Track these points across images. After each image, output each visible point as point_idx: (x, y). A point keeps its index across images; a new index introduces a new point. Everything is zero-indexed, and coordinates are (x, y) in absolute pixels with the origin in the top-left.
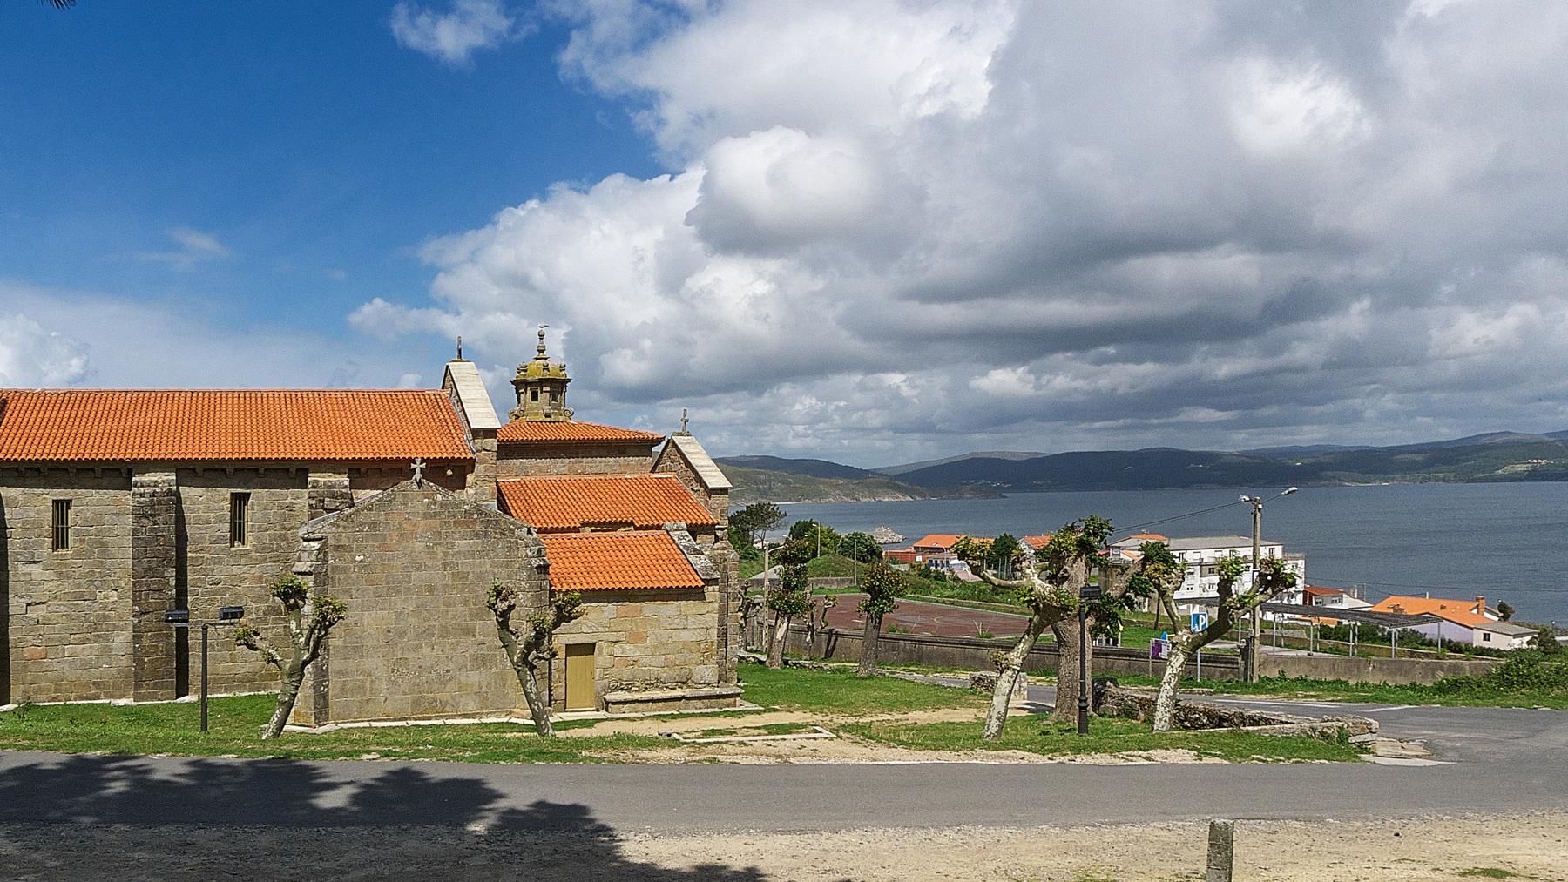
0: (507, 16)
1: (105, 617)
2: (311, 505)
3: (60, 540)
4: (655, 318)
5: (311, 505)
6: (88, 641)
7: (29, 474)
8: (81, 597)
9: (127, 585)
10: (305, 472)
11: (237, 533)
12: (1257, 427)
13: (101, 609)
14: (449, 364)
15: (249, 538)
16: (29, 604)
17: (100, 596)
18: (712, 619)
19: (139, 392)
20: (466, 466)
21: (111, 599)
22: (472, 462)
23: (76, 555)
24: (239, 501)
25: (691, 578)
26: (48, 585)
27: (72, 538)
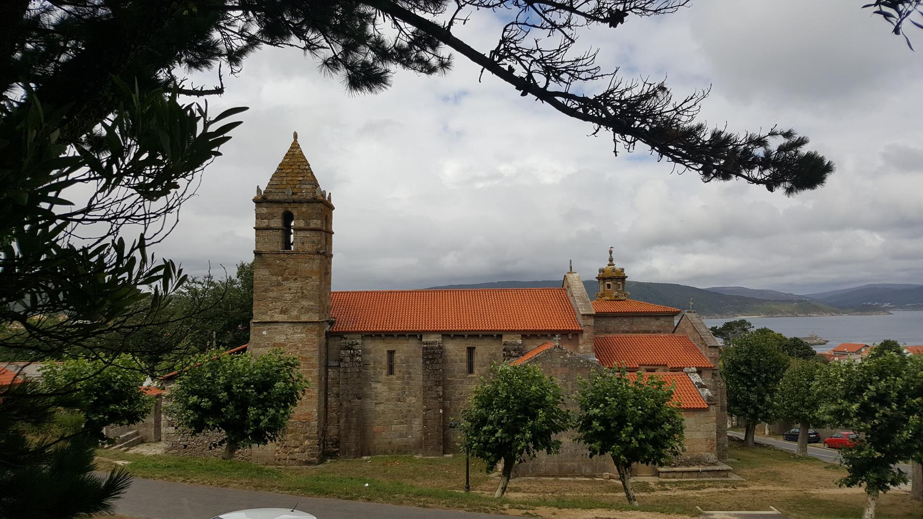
0: (731, 177)
1: (410, 411)
2: (504, 354)
3: (391, 371)
4: (371, 90)
5: (504, 354)
6: (402, 423)
7: (377, 337)
8: (399, 400)
9: (419, 394)
10: (500, 337)
11: (471, 371)
12: (56, 354)
13: (408, 407)
14: (566, 275)
15: (476, 371)
16: (376, 404)
17: (408, 400)
18: (713, 426)
19: (372, 292)
20: (577, 334)
21: (413, 401)
22: (582, 331)
23: (398, 378)
24: (471, 350)
25: (701, 403)
26: (385, 394)
27: (396, 370)
